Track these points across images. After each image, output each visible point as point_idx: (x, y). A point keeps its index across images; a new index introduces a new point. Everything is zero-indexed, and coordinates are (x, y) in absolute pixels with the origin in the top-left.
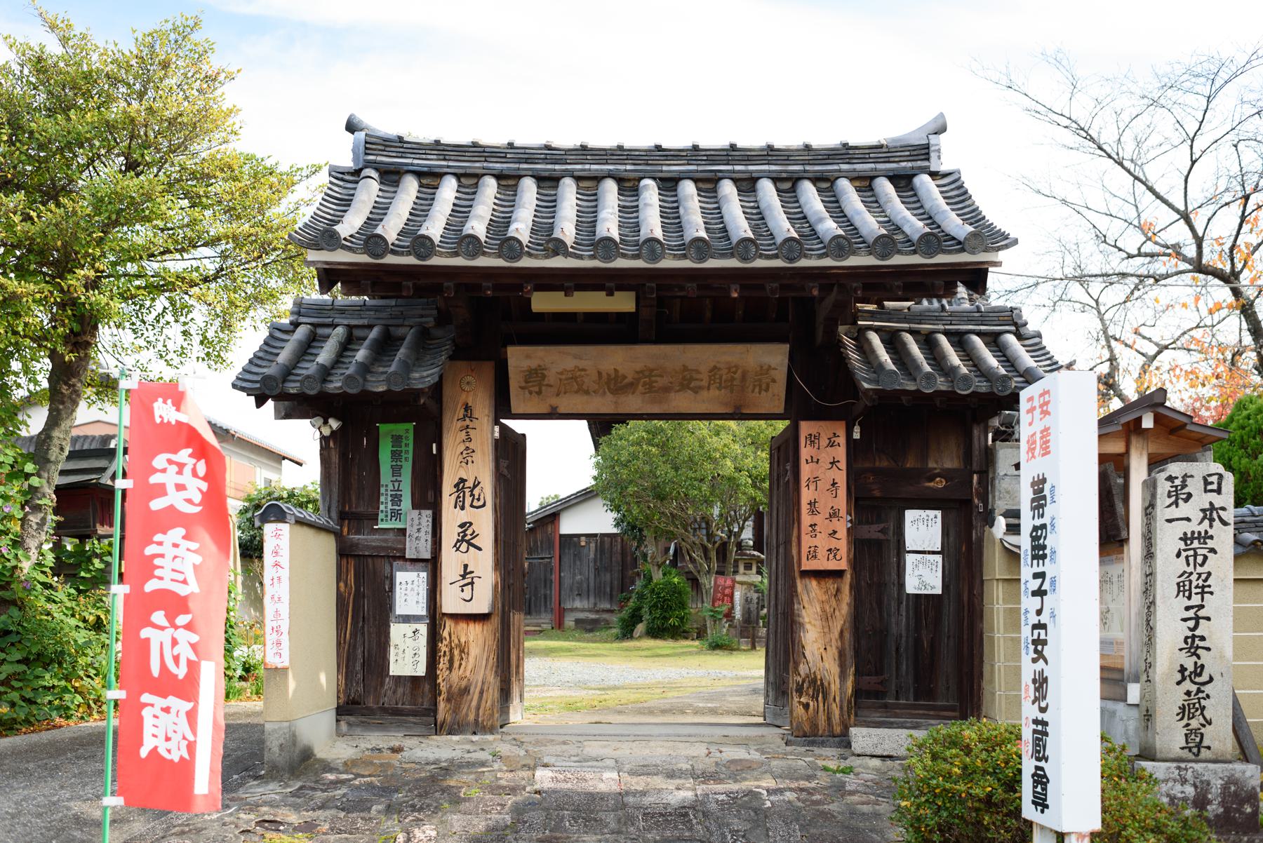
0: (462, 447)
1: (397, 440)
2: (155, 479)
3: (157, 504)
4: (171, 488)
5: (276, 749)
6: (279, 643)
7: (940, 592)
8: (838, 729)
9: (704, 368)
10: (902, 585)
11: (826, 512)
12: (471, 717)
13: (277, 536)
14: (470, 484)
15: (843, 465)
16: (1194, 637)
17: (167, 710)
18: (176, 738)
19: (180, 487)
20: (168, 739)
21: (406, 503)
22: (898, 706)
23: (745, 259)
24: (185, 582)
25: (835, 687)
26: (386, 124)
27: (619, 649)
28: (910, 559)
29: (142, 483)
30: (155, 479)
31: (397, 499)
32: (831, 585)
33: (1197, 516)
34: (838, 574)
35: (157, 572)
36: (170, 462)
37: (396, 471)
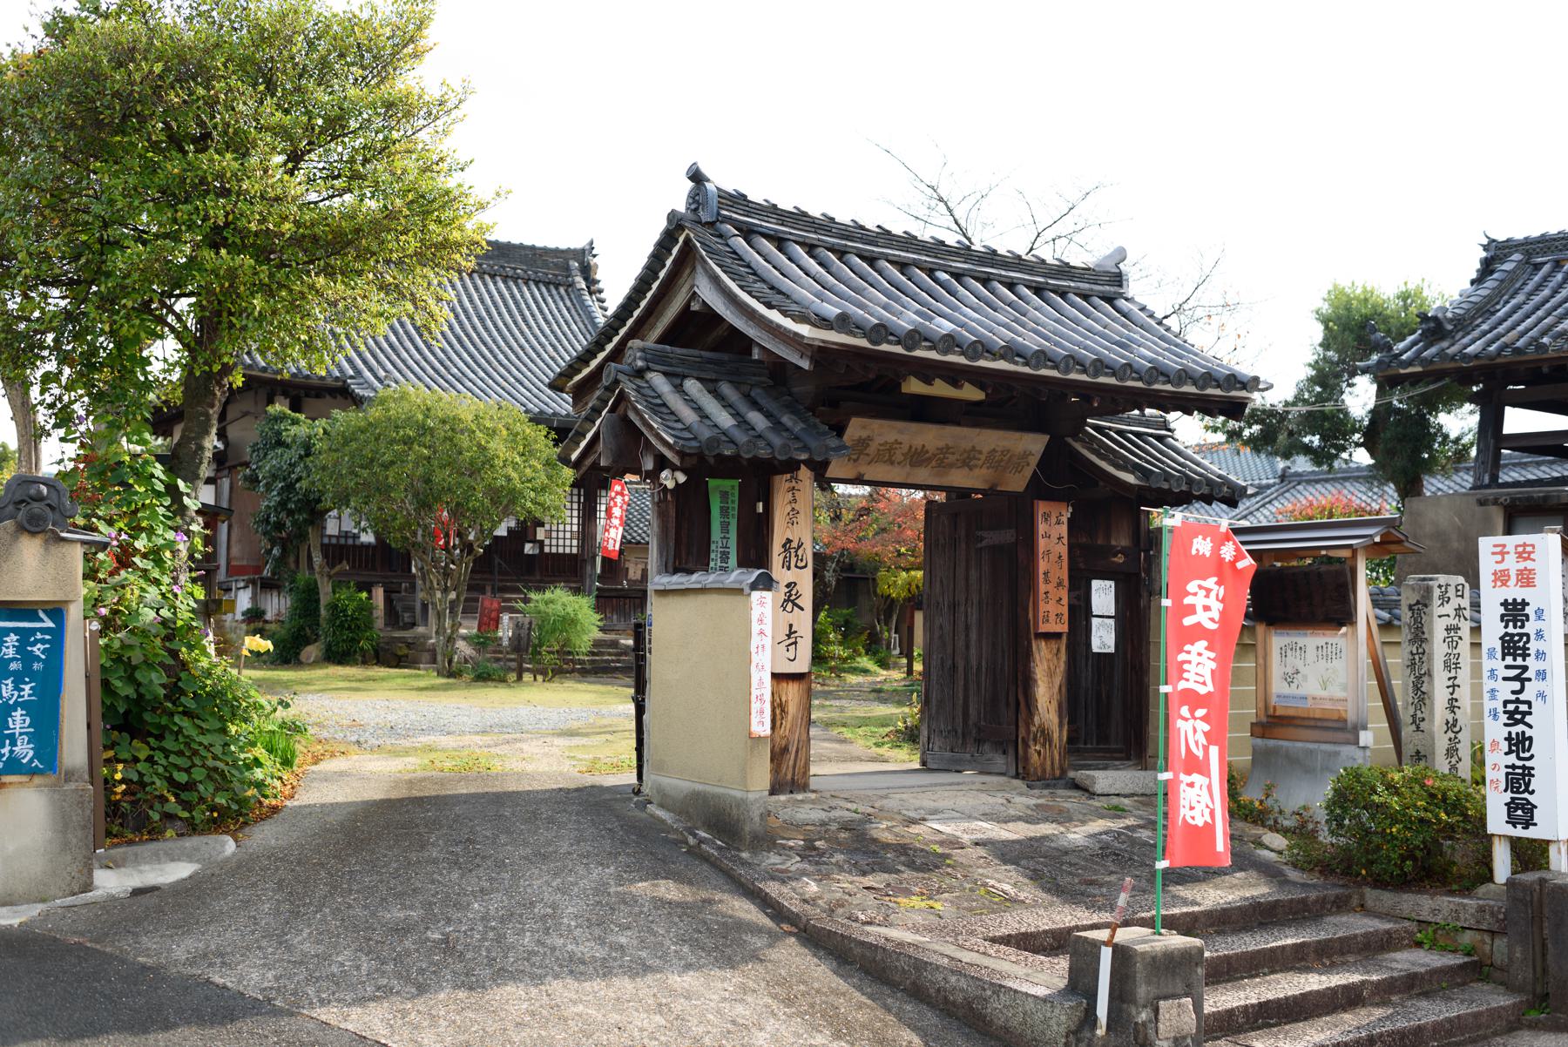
0: (789, 508)
1: (724, 495)
2: (1188, 600)
3: (1188, 621)
4: (1199, 609)
5: (757, 819)
6: (762, 712)
7: (1112, 650)
8: (1058, 773)
9: (985, 450)
10: (1089, 645)
11: (1055, 581)
12: (789, 777)
13: (762, 604)
14: (795, 545)
15: (1065, 541)
16: (1517, 701)
17: (1191, 785)
18: (1199, 808)
19: (1207, 608)
20: (1192, 808)
21: (733, 560)
22: (1087, 751)
23: (1121, 380)
24: (1204, 683)
25: (1056, 736)
26: (722, 178)
27: (347, 678)
28: (1095, 621)
29: (1178, 602)
30: (1188, 600)
31: (725, 557)
32: (1054, 645)
33: (1453, 613)
34: (1057, 636)
35: (1185, 675)
36: (1200, 587)
37: (725, 527)
